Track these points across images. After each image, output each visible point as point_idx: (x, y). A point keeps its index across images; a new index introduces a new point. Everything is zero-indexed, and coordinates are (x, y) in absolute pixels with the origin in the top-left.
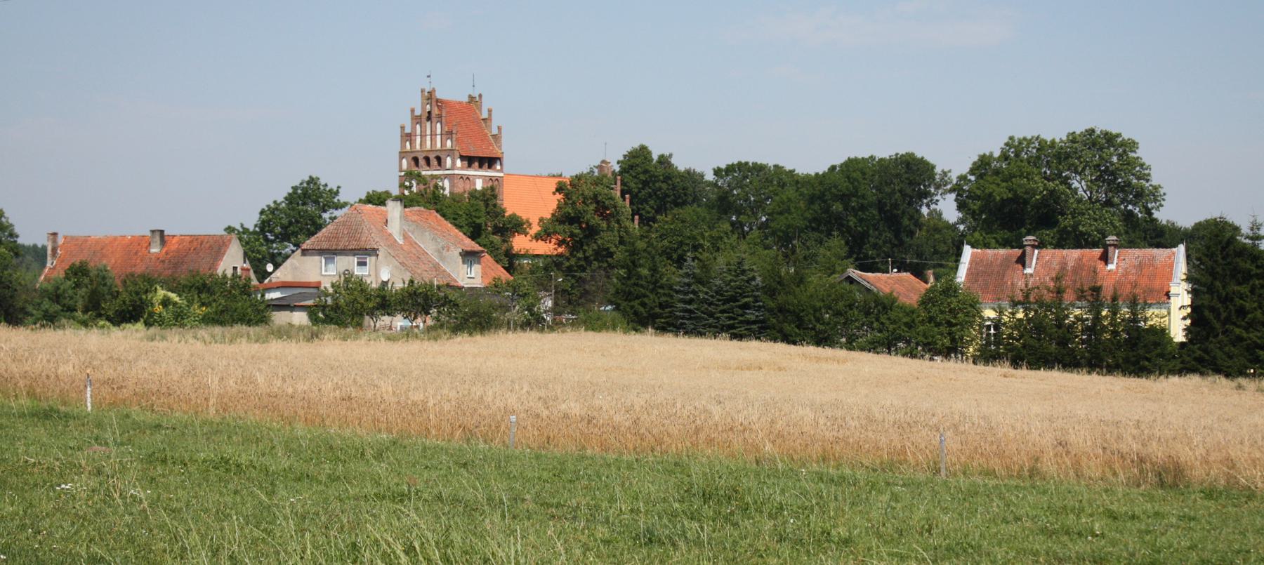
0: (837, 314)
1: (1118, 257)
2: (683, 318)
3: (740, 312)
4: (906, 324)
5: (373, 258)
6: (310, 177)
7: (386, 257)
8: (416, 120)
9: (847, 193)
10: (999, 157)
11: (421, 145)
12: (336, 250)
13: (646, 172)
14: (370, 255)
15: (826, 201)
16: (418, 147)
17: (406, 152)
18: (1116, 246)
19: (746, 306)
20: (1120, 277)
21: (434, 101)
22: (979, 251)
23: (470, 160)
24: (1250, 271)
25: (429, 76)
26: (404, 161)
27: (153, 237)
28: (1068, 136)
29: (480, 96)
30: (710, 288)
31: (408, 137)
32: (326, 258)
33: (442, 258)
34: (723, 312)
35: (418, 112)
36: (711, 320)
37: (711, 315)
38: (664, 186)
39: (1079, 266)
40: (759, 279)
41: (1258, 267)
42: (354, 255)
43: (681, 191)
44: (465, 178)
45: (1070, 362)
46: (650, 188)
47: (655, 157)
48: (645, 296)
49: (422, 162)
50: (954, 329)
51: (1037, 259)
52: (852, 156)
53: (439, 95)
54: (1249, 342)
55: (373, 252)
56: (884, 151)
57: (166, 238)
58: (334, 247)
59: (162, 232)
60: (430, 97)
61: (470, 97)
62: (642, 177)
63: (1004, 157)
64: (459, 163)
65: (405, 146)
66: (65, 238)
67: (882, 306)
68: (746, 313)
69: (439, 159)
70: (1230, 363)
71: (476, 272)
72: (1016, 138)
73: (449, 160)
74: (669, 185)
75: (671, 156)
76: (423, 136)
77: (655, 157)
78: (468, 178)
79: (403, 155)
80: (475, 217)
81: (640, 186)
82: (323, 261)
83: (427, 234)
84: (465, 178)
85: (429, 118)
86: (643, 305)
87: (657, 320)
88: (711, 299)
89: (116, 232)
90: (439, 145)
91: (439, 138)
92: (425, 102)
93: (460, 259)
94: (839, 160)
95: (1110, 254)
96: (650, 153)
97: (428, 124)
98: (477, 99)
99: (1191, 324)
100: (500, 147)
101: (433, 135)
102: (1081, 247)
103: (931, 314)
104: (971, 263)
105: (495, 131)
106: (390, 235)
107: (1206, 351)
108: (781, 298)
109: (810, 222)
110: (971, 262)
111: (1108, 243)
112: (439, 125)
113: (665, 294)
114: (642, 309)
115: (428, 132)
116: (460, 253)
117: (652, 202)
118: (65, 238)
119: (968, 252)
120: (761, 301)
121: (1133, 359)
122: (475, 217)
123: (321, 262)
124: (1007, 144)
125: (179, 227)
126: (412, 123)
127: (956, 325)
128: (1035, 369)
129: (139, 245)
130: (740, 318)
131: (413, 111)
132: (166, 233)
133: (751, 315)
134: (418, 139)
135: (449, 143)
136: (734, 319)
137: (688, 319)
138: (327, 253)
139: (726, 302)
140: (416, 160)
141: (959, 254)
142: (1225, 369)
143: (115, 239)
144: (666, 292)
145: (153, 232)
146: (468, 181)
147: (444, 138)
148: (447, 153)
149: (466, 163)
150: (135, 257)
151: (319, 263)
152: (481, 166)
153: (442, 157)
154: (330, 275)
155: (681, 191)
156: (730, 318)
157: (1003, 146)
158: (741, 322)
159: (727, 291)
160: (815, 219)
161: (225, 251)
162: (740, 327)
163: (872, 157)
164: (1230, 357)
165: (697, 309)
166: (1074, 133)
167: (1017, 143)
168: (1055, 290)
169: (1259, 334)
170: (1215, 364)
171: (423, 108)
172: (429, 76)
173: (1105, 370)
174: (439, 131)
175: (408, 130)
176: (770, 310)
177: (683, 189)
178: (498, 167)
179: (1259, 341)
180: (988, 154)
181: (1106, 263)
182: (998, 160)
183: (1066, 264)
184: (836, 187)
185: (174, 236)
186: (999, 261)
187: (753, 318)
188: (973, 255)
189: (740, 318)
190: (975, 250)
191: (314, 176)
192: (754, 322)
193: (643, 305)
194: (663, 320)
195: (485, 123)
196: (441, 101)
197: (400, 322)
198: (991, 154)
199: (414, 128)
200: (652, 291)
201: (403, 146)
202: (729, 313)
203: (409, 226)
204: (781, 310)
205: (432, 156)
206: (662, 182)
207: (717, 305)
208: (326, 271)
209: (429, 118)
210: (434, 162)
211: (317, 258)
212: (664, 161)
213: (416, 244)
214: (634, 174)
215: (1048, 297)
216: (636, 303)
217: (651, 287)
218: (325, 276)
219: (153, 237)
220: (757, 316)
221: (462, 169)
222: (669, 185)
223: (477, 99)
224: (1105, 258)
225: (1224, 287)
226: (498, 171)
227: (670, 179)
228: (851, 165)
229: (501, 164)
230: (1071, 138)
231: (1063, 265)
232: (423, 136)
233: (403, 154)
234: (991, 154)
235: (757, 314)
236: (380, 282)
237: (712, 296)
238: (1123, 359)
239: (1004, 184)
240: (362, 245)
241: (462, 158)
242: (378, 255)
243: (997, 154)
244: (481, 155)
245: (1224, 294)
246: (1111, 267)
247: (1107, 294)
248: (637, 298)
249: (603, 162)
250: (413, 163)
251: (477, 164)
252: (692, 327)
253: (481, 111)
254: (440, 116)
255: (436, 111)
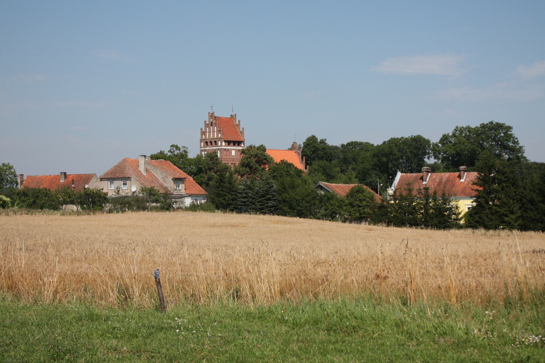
0: (307, 202)
1: (466, 176)
2: (241, 205)
3: (266, 202)
4: (338, 207)
5: (129, 181)
6: (161, 151)
7: (134, 181)
8: (206, 125)
9: (388, 153)
10: (452, 136)
11: (209, 136)
12: (113, 178)
13: (314, 147)
14: (128, 180)
15: (379, 156)
16: (208, 137)
17: (203, 139)
18: (465, 171)
19: (269, 199)
20: (465, 186)
21: (213, 117)
22: (404, 174)
23: (229, 143)
24: (501, 179)
25: (212, 107)
26: (202, 143)
27: (61, 175)
28: (481, 125)
29: (235, 115)
30: (253, 191)
31: (203, 133)
32: (110, 182)
33: (165, 181)
34: (259, 202)
35: (207, 122)
36: (253, 206)
37: (253, 203)
38: (322, 153)
39: (448, 180)
40: (275, 186)
41: (505, 177)
42: (122, 180)
43: (329, 155)
44: (227, 150)
45: (414, 223)
46: (316, 154)
47: (319, 140)
48: (226, 195)
49: (209, 144)
50: (360, 208)
51: (430, 177)
52: (393, 137)
53: (216, 115)
54: (501, 213)
55: (129, 179)
56: (407, 134)
57: (67, 176)
58: (113, 177)
59: (65, 173)
60: (212, 115)
61: (231, 115)
62: (312, 149)
63: (454, 135)
64: (224, 144)
65: (203, 137)
66: (28, 176)
67: (330, 197)
68: (269, 203)
69: (215, 142)
70: (491, 223)
71: (182, 187)
72: (459, 128)
73: (219, 142)
74: (324, 152)
75: (325, 140)
76: (210, 132)
77: (319, 140)
78: (228, 150)
79: (202, 141)
80: (199, 164)
81: (311, 153)
82: (109, 183)
83: (158, 171)
84: (227, 150)
85: (212, 125)
86: (224, 199)
87: (231, 207)
88: (254, 196)
89: (48, 174)
90: (216, 136)
91: (215, 133)
92: (210, 118)
93: (172, 182)
94: (387, 139)
95: (462, 175)
96: (317, 139)
97: (211, 127)
98: (234, 116)
99: (477, 205)
100: (243, 137)
101: (214, 132)
102: (450, 172)
103: (350, 202)
104: (400, 180)
105: (241, 130)
106: (140, 171)
107: (480, 218)
108: (284, 195)
109: (373, 166)
110: (400, 179)
111: (460, 169)
112: (215, 127)
113: (234, 195)
114: (223, 201)
115: (212, 131)
116: (172, 179)
117: (206, 153)
118: (28, 176)
119: (399, 175)
120: (275, 197)
121: (443, 222)
122: (199, 164)
123: (108, 184)
124: (455, 130)
125: (72, 171)
126: (205, 127)
127: (362, 206)
128: (398, 227)
129: (56, 179)
130: (266, 205)
131: (205, 122)
132: (67, 174)
133: (270, 204)
134: (208, 134)
135: (220, 135)
136: (264, 205)
137: (243, 206)
138: (111, 180)
139: (260, 197)
140: (207, 143)
141: (396, 174)
142: (489, 226)
143: (47, 177)
144: (235, 193)
145: (61, 173)
146: (228, 151)
147: (218, 133)
148: (219, 139)
149: (227, 144)
150: (54, 184)
151: (107, 184)
152: (234, 145)
153: (217, 141)
154: (112, 189)
155: (329, 155)
156: (261, 205)
157: (453, 131)
158: (267, 207)
159: (261, 192)
160: (375, 165)
161: (90, 181)
162: (266, 209)
163: (402, 137)
164: (491, 220)
165: (247, 201)
166: (484, 124)
167: (459, 129)
168: (408, 189)
169: (505, 209)
170: (484, 224)
171: (209, 121)
172: (212, 107)
173: (430, 227)
174: (215, 130)
175: (203, 130)
176: (279, 201)
177: (330, 154)
178: (243, 145)
179: (504, 213)
180: (447, 134)
181: (460, 179)
182: (451, 137)
183: (442, 179)
184: (383, 150)
185: (70, 175)
186: (412, 179)
187: (271, 205)
188: (402, 176)
189: (266, 205)
190: (403, 174)
191: (162, 150)
192: (272, 207)
193: (224, 199)
194: (233, 206)
195: (237, 126)
196: (217, 117)
197: (74, 208)
198: (448, 134)
199: (206, 129)
200: (229, 193)
201: (202, 137)
202: (261, 202)
203: (151, 167)
204: (284, 201)
205: (213, 141)
206: (321, 151)
207: (257, 199)
208: (110, 187)
209: (212, 125)
210: (214, 144)
211: (106, 182)
212: (323, 142)
213: (153, 175)
214: (309, 148)
215: (404, 193)
216: (221, 199)
217: (229, 191)
218: (110, 190)
219: (61, 175)
220: (274, 204)
221: (225, 146)
222: (324, 152)
223: (234, 116)
224: (460, 177)
225: (489, 187)
226: (242, 147)
227: (325, 149)
228: (393, 141)
229: (244, 144)
230: (482, 126)
231: (441, 180)
232: (210, 132)
233: (201, 140)
234: (448, 134)
235: (273, 203)
236: (132, 192)
237: (254, 195)
238: (438, 222)
239: (453, 147)
240: (125, 175)
241: (225, 141)
242: (131, 180)
243: (451, 134)
244: (234, 140)
245: (489, 190)
246: (462, 180)
247: (431, 192)
248: (222, 196)
249: (294, 143)
250: (205, 144)
251: (232, 144)
252: (246, 209)
253: (236, 121)
254: (216, 124)
255: (214, 121)
